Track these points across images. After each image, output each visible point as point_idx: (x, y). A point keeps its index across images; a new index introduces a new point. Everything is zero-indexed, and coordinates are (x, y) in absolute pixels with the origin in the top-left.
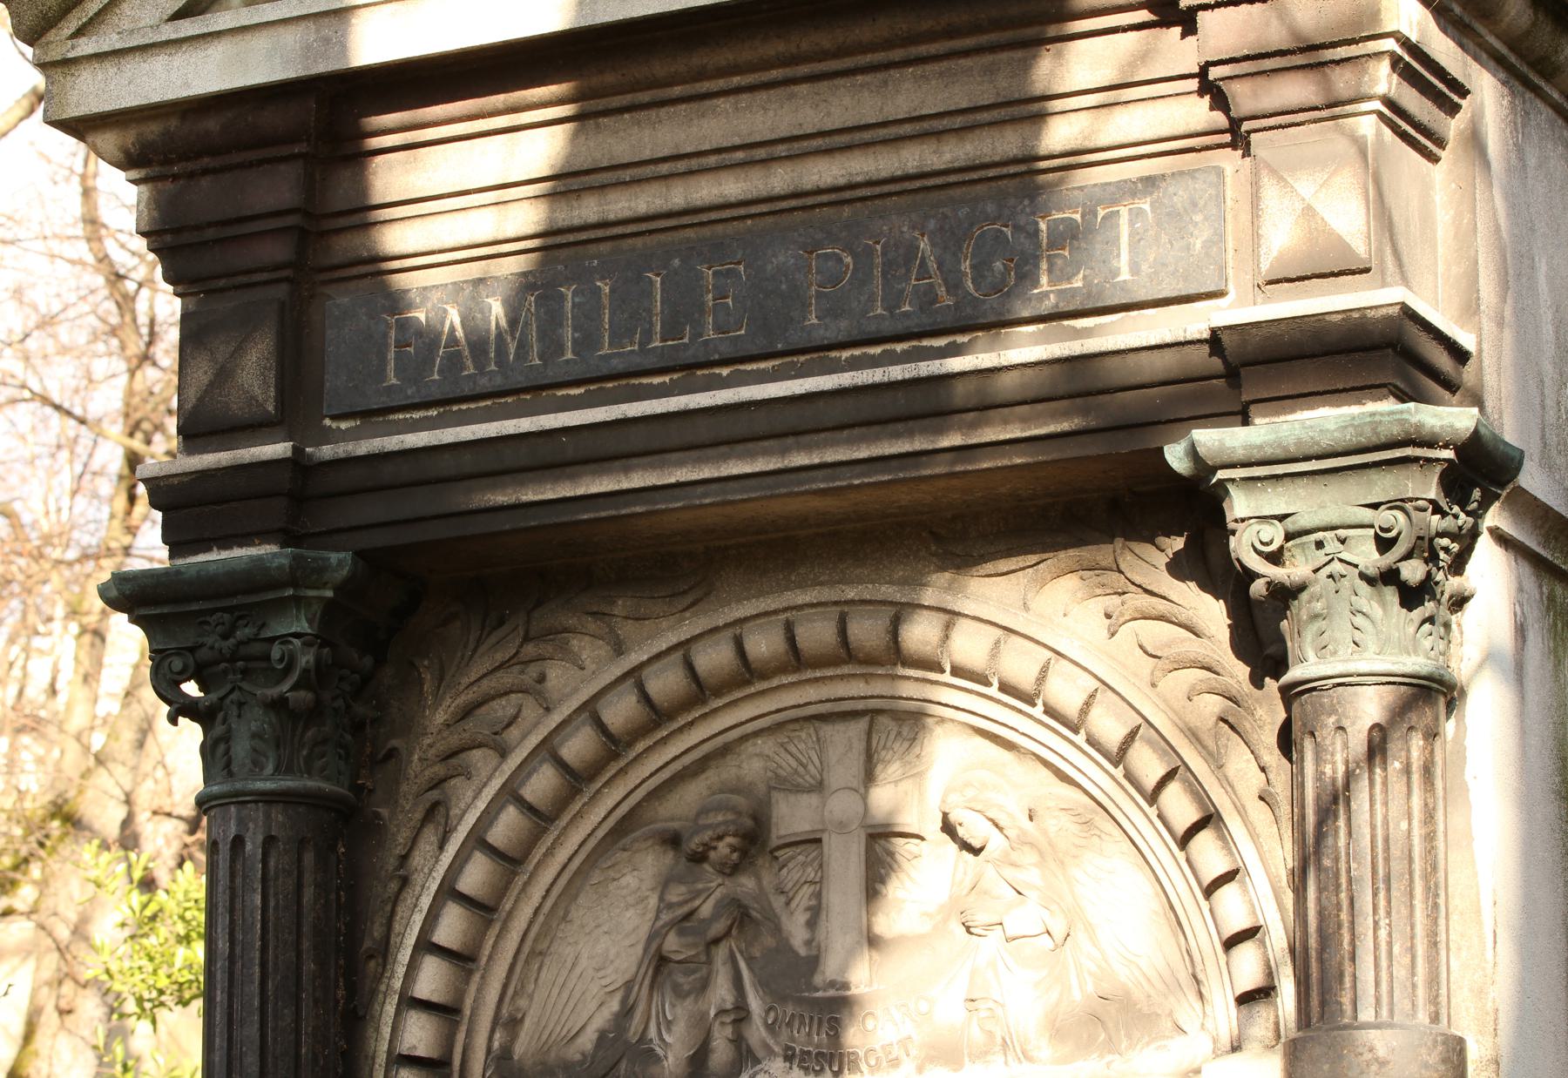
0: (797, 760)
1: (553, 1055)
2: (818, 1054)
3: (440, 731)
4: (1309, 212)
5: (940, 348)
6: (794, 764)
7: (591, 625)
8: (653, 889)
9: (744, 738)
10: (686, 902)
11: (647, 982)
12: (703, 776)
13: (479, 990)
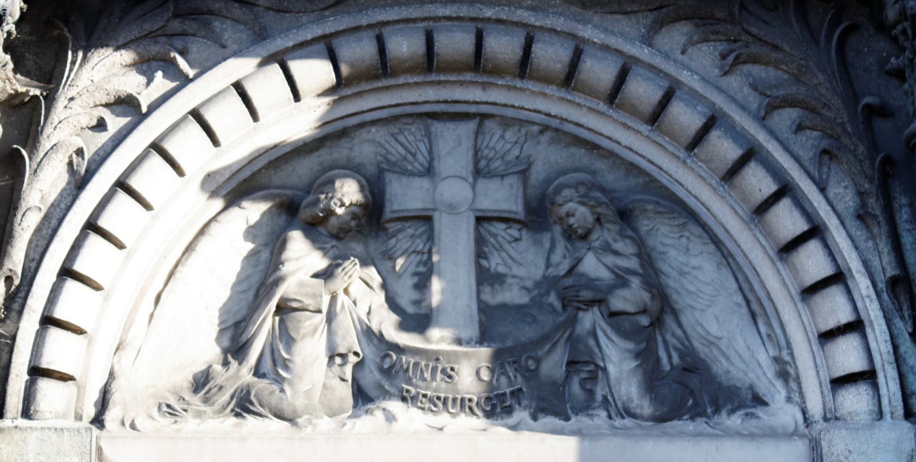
0: (406, 148)
6: (403, 152)
7: (237, 10)
9: (362, 125)
12: (316, 154)
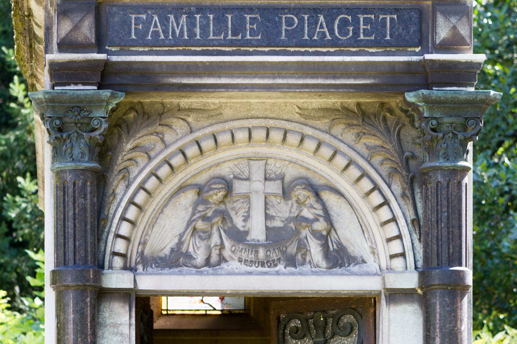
0: (240, 170)
1: (155, 254)
2: (250, 261)
3: (128, 151)
4: (454, 28)
5: (324, 52)
8: (190, 206)
10: (204, 211)
11: (190, 234)
13: (136, 233)
